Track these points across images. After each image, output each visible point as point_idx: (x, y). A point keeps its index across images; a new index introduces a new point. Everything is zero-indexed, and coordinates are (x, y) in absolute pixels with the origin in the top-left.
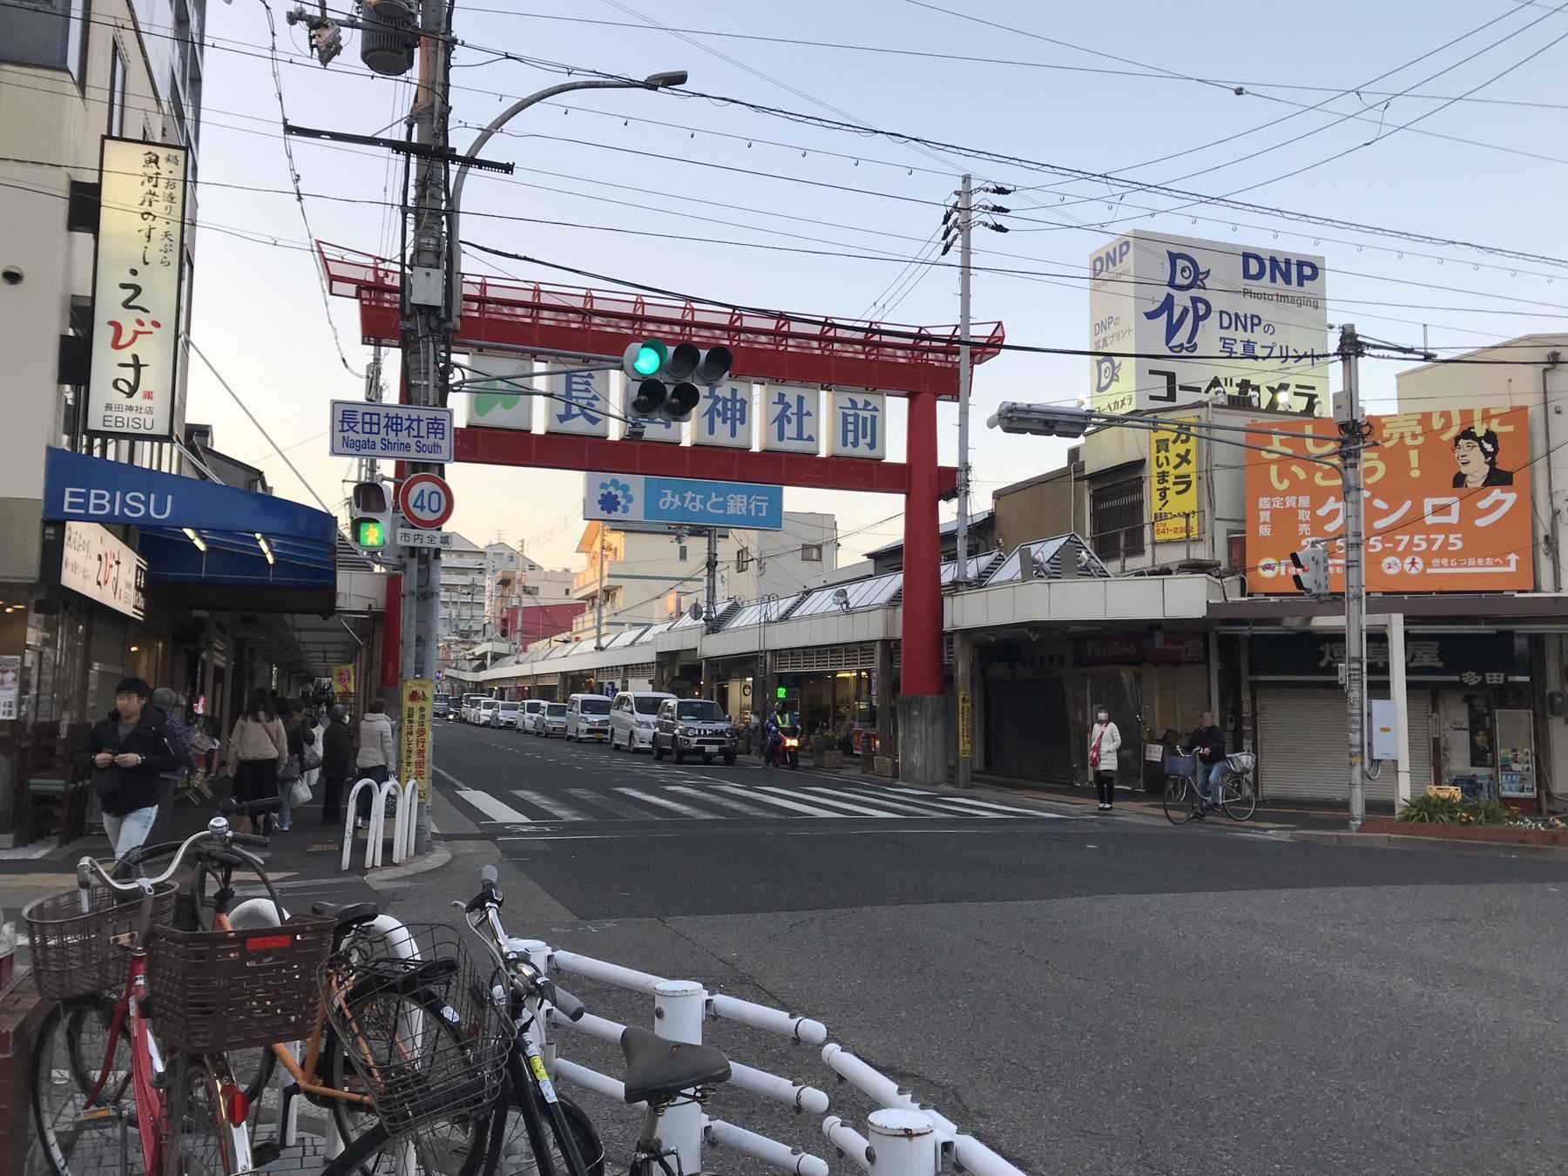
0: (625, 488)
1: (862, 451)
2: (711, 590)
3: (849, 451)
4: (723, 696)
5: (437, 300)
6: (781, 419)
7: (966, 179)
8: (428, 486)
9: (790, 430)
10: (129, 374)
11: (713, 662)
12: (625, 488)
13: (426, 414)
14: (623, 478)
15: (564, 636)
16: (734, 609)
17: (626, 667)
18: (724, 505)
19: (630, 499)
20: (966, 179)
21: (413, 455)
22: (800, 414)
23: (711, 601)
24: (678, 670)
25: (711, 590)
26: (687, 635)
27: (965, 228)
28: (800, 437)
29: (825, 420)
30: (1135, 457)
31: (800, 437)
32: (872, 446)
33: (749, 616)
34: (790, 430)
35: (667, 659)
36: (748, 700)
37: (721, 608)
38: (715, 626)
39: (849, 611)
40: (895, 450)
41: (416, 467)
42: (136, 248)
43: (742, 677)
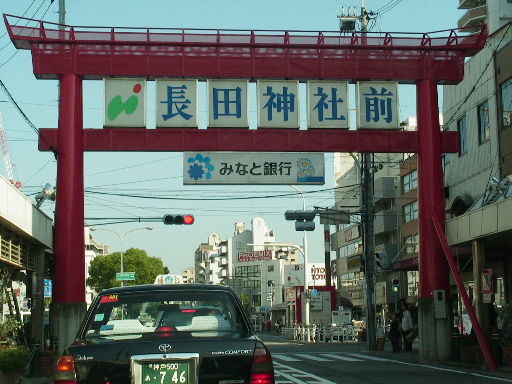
6: (321, 106)
9: (328, 113)
22: (334, 101)
28: (335, 117)
31: (335, 117)
32: (389, 120)
34: (328, 113)
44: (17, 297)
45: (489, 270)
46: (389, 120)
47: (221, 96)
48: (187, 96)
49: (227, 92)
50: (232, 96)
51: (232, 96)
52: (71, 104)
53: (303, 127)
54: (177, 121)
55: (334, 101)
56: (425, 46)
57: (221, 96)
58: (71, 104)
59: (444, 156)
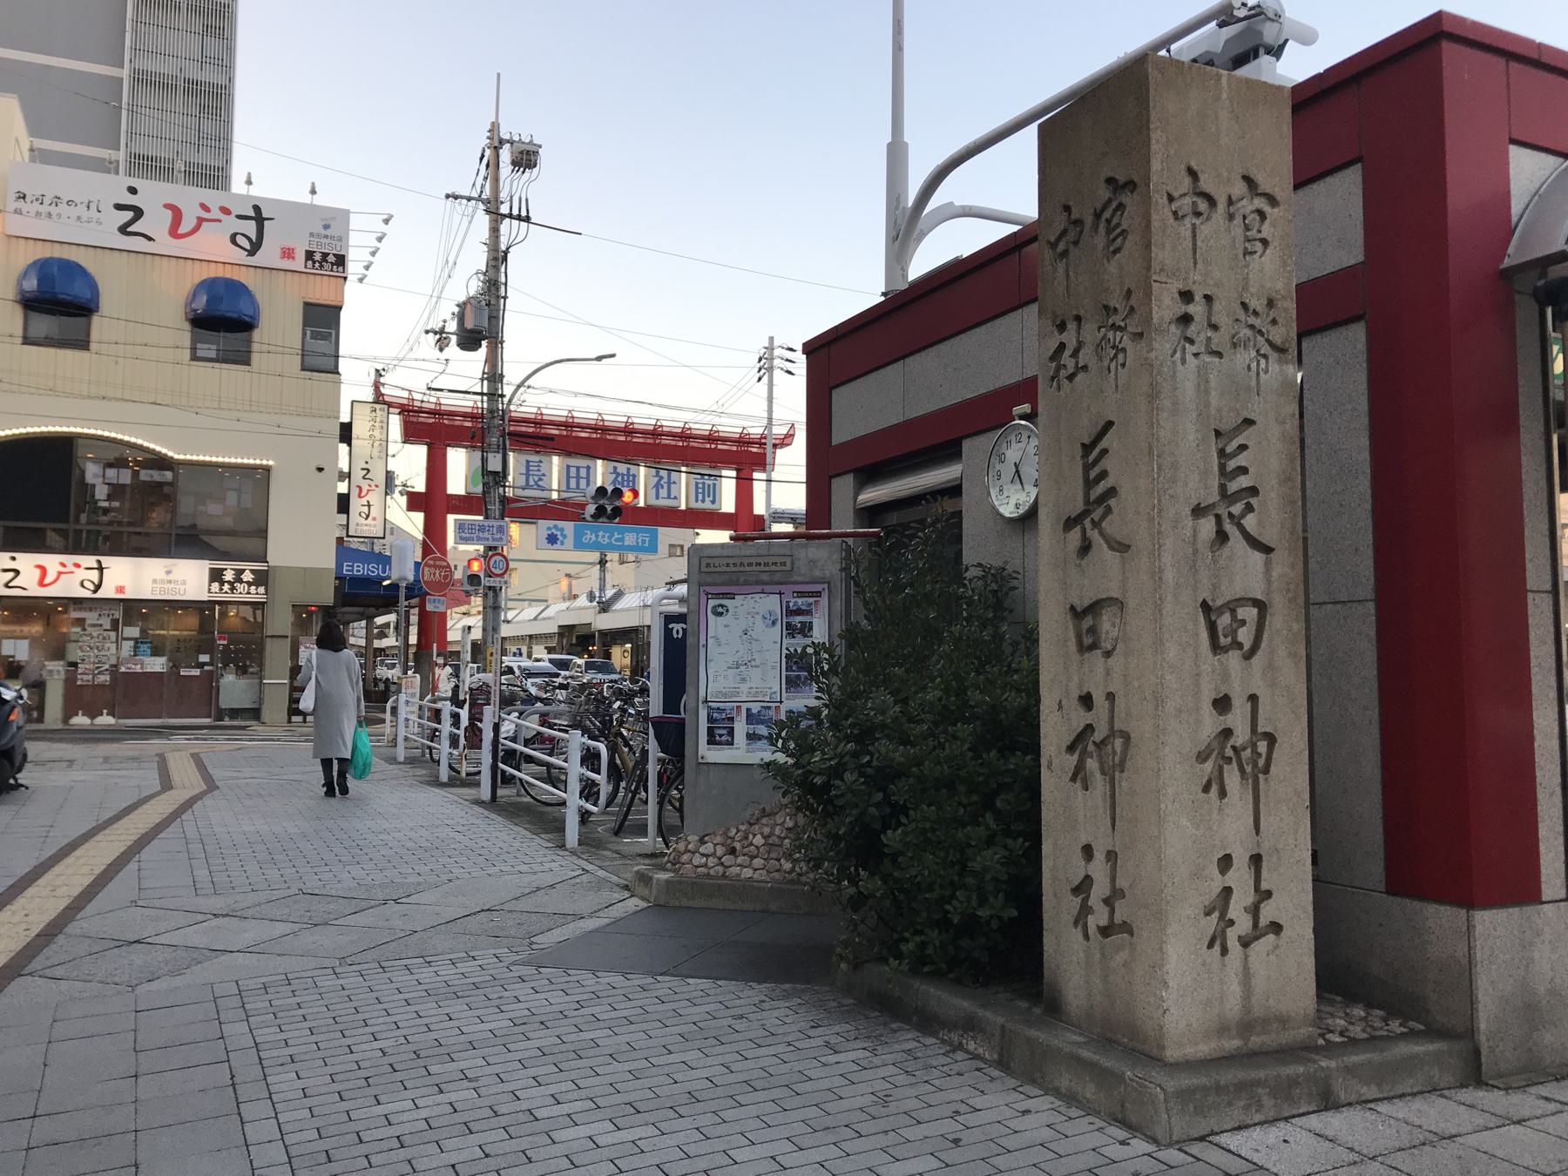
0: (562, 530)
1: (707, 505)
2: (603, 580)
3: (699, 505)
4: (608, 656)
5: (499, 469)
6: (658, 486)
7: (771, 339)
8: (498, 558)
9: (663, 493)
10: (366, 509)
11: (603, 633)
12: (562, 530)
13: (496, 523)
14: (560, 524)
15: (463, 609)
16: (619, 595)
17: (531, 636)
18: (622, 540)
19: (565, 537)
20: (771, 339)
21: (491, 543)
22: (669, 483)
23: (602, 588)
24: (576, 639)
25: (603, 580)
26: (582, 612)
27: (770, 369)
28: (669, 497)
29: (683, 489)
30: (1301, 192)
31: (669, 497)
32: (713, 502)
33: (630, 601)
34: (663, 493)
35: (565, 630)
36: (628, 661)
37: (609, 593)
38: (605, 607)
39: (487, 1156)
40: (728, 505)
41: (490, 548)
42: (368, 452)
43: (623, 644)
44: (302, 649)
45: (724, 473)
46: (713, 502)
47: (573, 471)
48: (543, 470)
49: (578, 468)
50: (583, 473)
51: (583, 473)
52: (436, 470)
53: (683, 507)
54: (663, 502)
55: (669, 483)
56: (743, 440)
57: (573, 471)
58: (436, 470)
59: (799, 668)
